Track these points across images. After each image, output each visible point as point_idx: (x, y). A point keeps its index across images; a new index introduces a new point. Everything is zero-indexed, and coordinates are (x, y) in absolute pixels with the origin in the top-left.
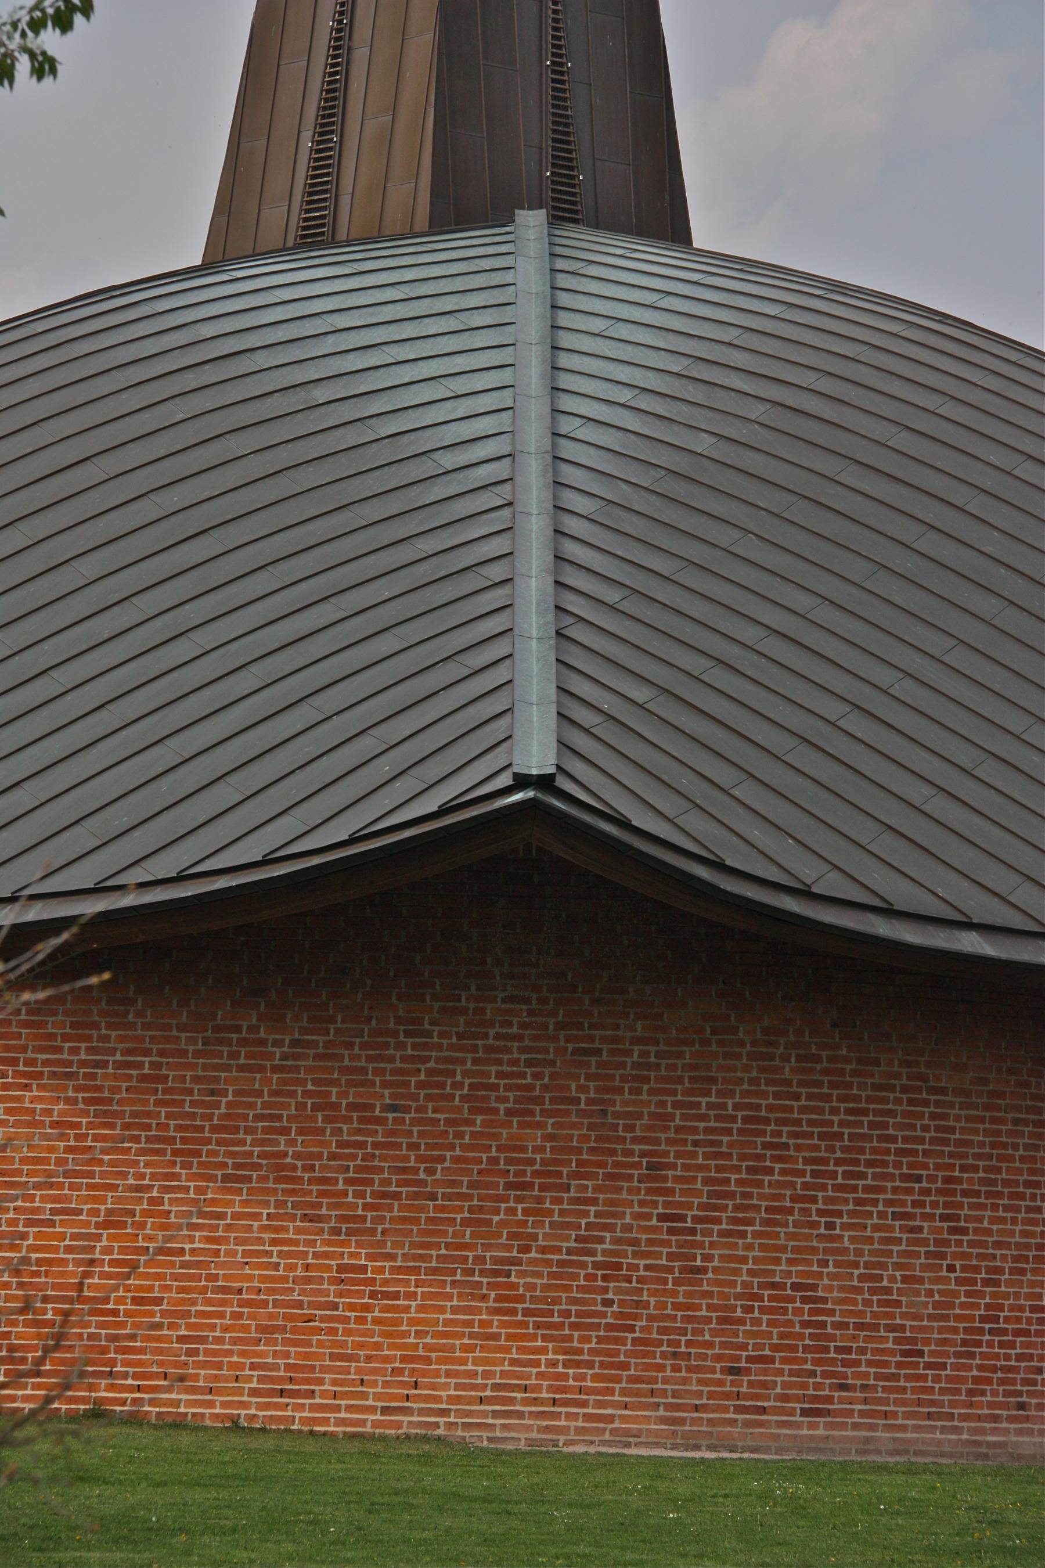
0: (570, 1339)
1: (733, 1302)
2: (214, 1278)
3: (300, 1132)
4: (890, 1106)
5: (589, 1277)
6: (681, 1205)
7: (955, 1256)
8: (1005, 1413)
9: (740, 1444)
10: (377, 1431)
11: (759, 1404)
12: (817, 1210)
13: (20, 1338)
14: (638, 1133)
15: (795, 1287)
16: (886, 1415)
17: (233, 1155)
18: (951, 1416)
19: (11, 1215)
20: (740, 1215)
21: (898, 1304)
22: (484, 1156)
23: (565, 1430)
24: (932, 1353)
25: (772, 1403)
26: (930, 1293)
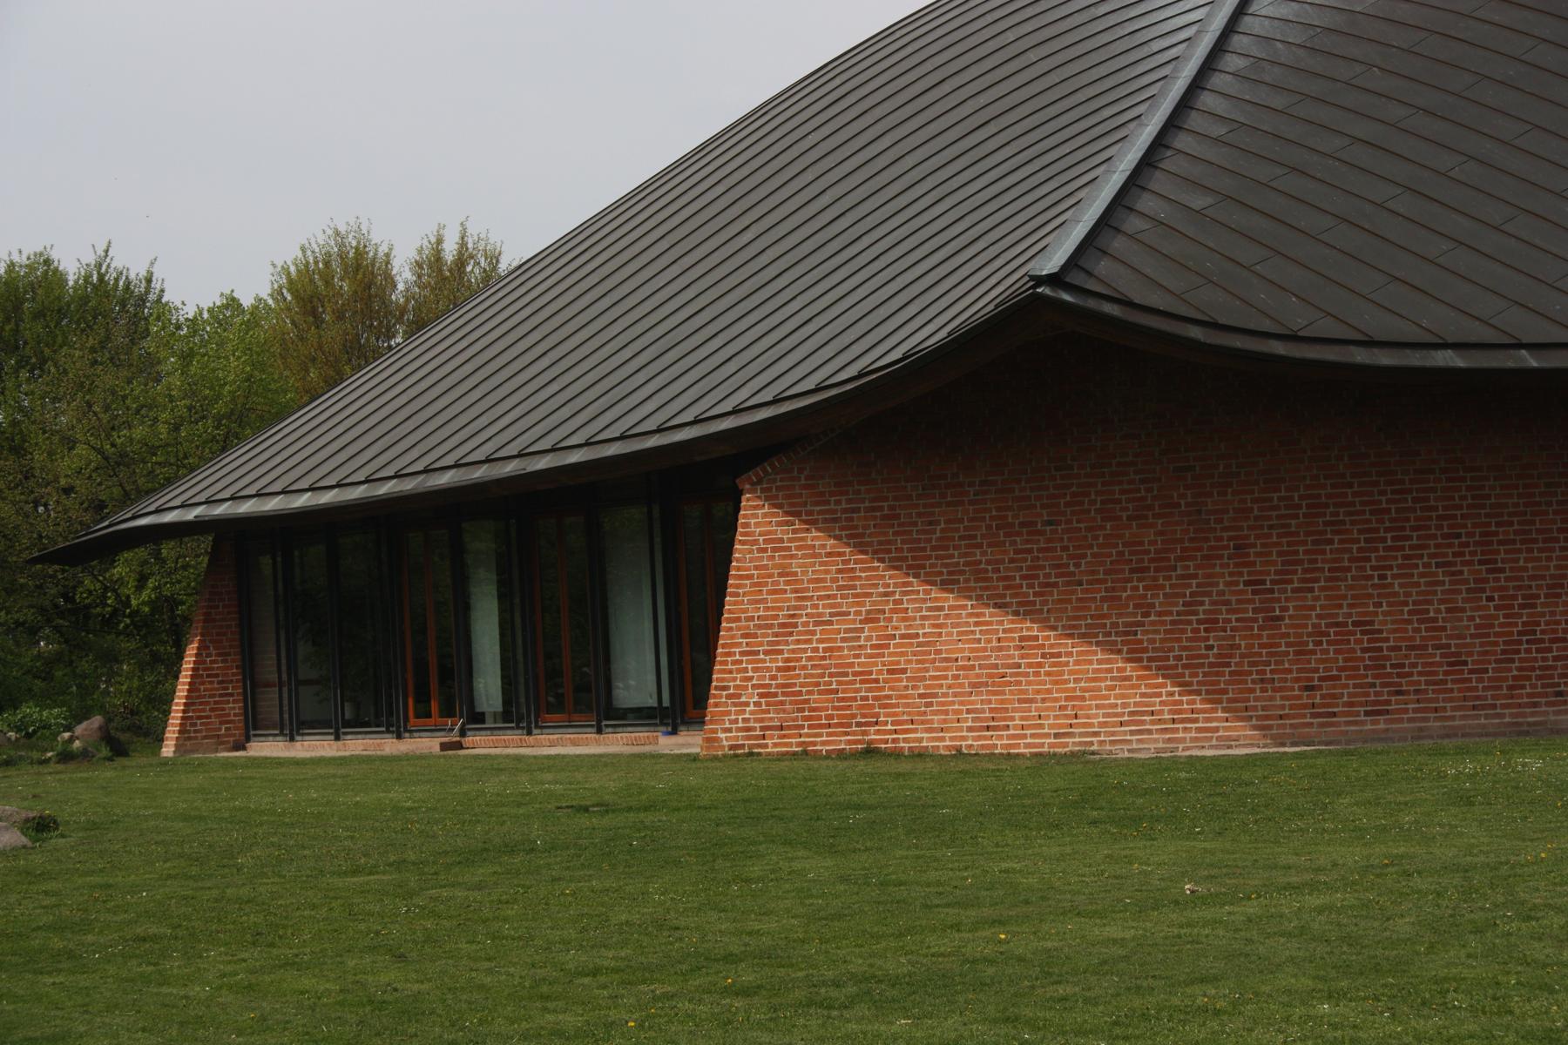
0: (1183, 675)
1: (1305, 639)
2: (938, 652)
3: (990, 545)
4: (1431, 485)
5: (1194, 631)
6: (1261, 573)
7: (1493, 589)
8: (1544, 700)
9: (1316, 740)
10: (1052, 750)
11: (1330, 710)
12: (1371, 567)
13: (816, 703)
14: (1226, 524)
15: (1355, 624)
16: (1436, 710)
17: (946, 565)
18: (1494, 706)
19: (804, 619)
20: (1309, 576)
21: (1444, 629)
22: (1114, 551)
23: (1183, 740)
24: (1474, 662)
25: (1340, 709)
26: (1471, 618)
